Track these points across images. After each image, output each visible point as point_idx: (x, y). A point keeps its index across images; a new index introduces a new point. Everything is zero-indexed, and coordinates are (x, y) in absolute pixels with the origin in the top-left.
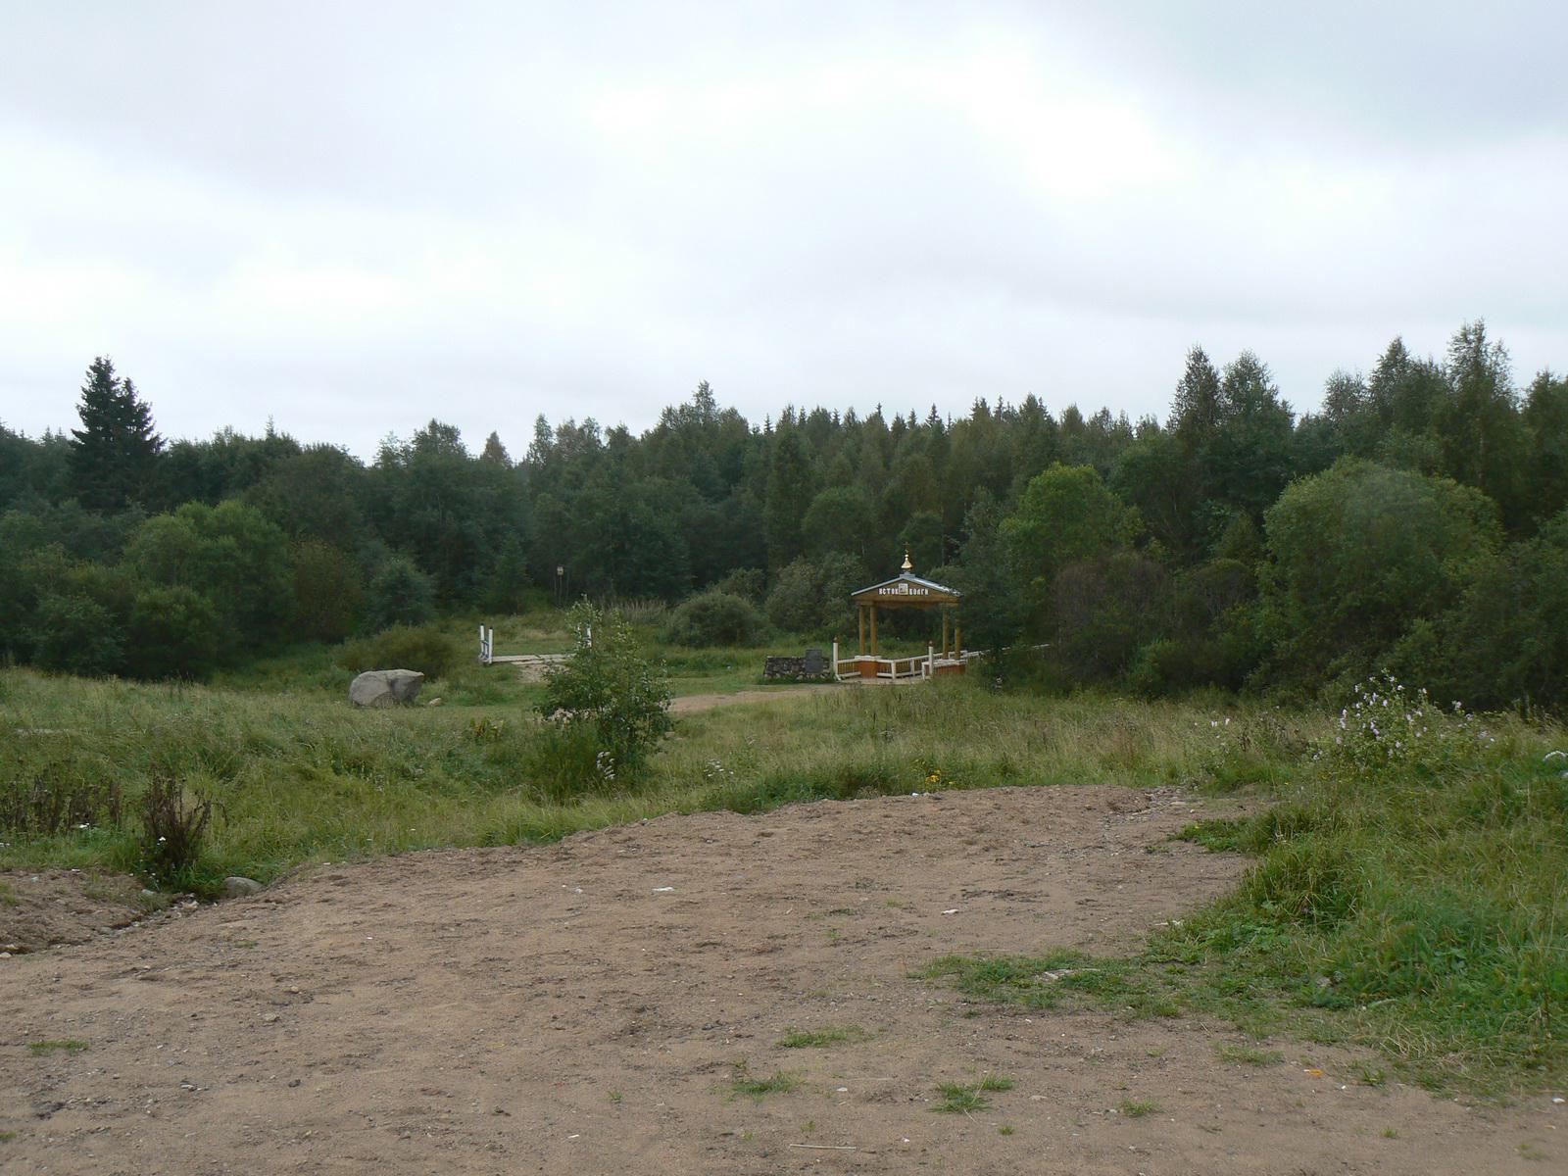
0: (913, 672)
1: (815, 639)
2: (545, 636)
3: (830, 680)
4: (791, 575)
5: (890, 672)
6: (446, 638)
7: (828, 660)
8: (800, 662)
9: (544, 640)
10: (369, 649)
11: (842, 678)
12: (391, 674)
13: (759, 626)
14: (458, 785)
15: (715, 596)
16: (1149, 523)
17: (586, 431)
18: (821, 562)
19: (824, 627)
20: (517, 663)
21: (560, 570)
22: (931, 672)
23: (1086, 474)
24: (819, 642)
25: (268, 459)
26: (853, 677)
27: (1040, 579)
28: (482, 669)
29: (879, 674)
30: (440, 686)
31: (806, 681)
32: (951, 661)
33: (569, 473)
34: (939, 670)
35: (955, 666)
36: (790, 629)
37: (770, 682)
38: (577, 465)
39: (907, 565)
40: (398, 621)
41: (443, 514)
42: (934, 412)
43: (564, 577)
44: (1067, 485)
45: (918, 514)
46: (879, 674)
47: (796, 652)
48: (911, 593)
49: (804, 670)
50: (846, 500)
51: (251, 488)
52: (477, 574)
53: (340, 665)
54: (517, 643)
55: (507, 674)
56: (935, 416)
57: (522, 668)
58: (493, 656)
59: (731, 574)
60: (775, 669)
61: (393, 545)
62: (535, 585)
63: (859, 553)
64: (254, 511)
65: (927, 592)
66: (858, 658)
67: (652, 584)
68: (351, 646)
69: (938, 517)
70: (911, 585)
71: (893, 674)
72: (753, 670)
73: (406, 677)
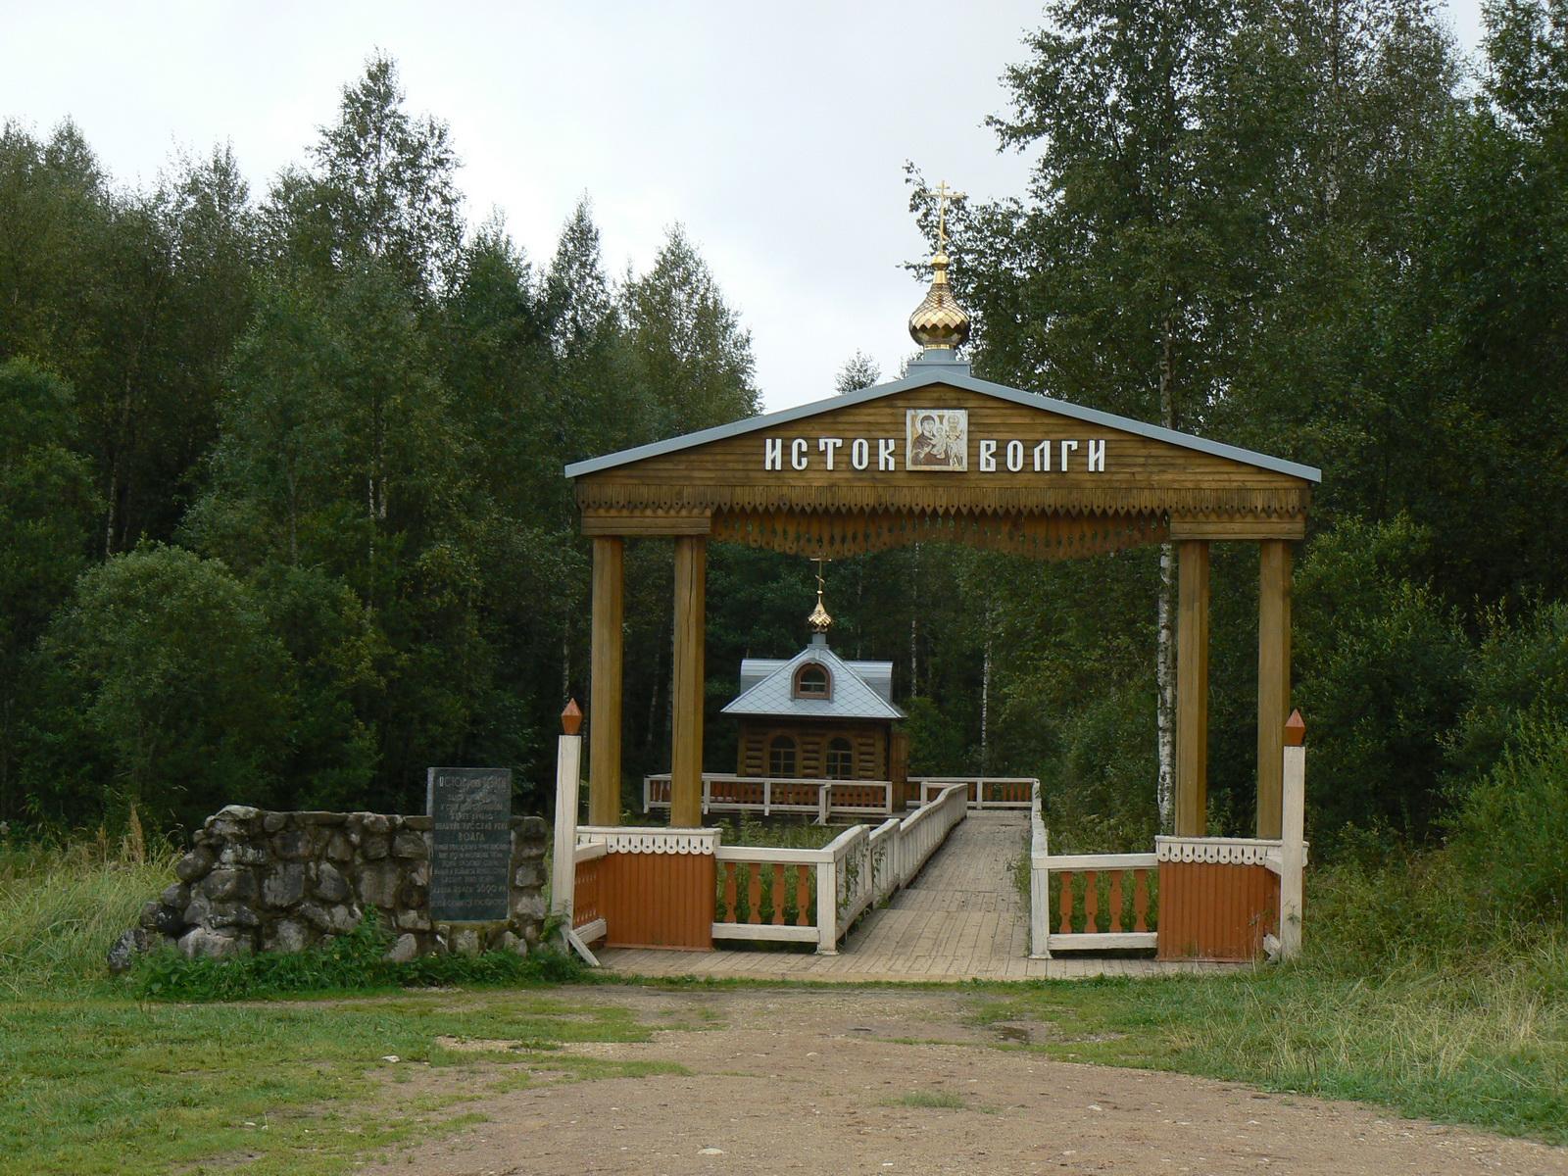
16: (37, 763)
48: (987, 463)
60: (276, 891)
65: (1097, 457)
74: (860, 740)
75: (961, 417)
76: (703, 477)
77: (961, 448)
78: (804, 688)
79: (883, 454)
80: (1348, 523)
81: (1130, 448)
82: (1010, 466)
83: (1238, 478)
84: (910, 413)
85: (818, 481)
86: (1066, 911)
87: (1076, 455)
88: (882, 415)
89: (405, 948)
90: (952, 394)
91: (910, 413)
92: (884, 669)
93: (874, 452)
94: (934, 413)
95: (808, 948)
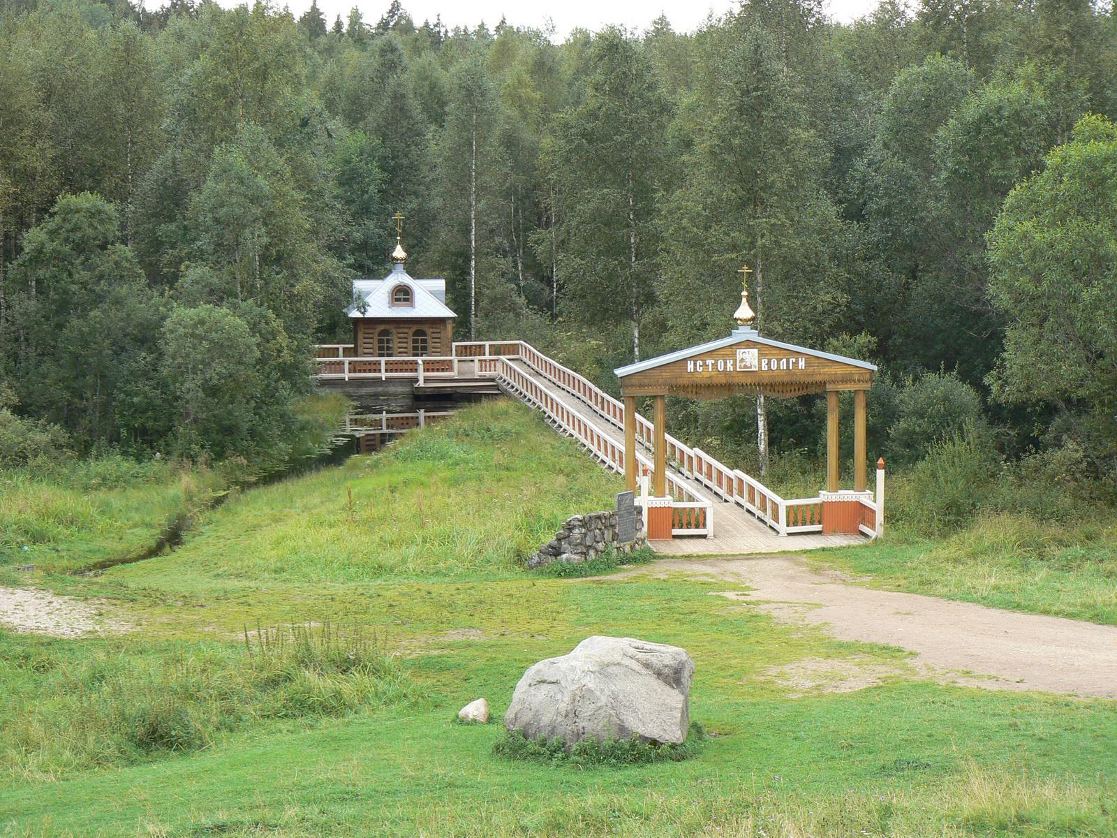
29: (676, 532)
46: (676, 532)
65: (802, 364)
74: (431, 330)
75: (756, 351)
77: (756, 362)
78: (397, 300)
79: (729, 365)
80: (845, 336)
81: (813, 360)
82: (772, 368)
83: (849, 370)
84: (738, 351)
85: (706, 375)
86: (792, 520)
88: (728, 352)
90: (751, 343)
91: (738, 351)
92: (440, 284)
93: (725, 364)
94: (746, 350)
95: (704, 537)
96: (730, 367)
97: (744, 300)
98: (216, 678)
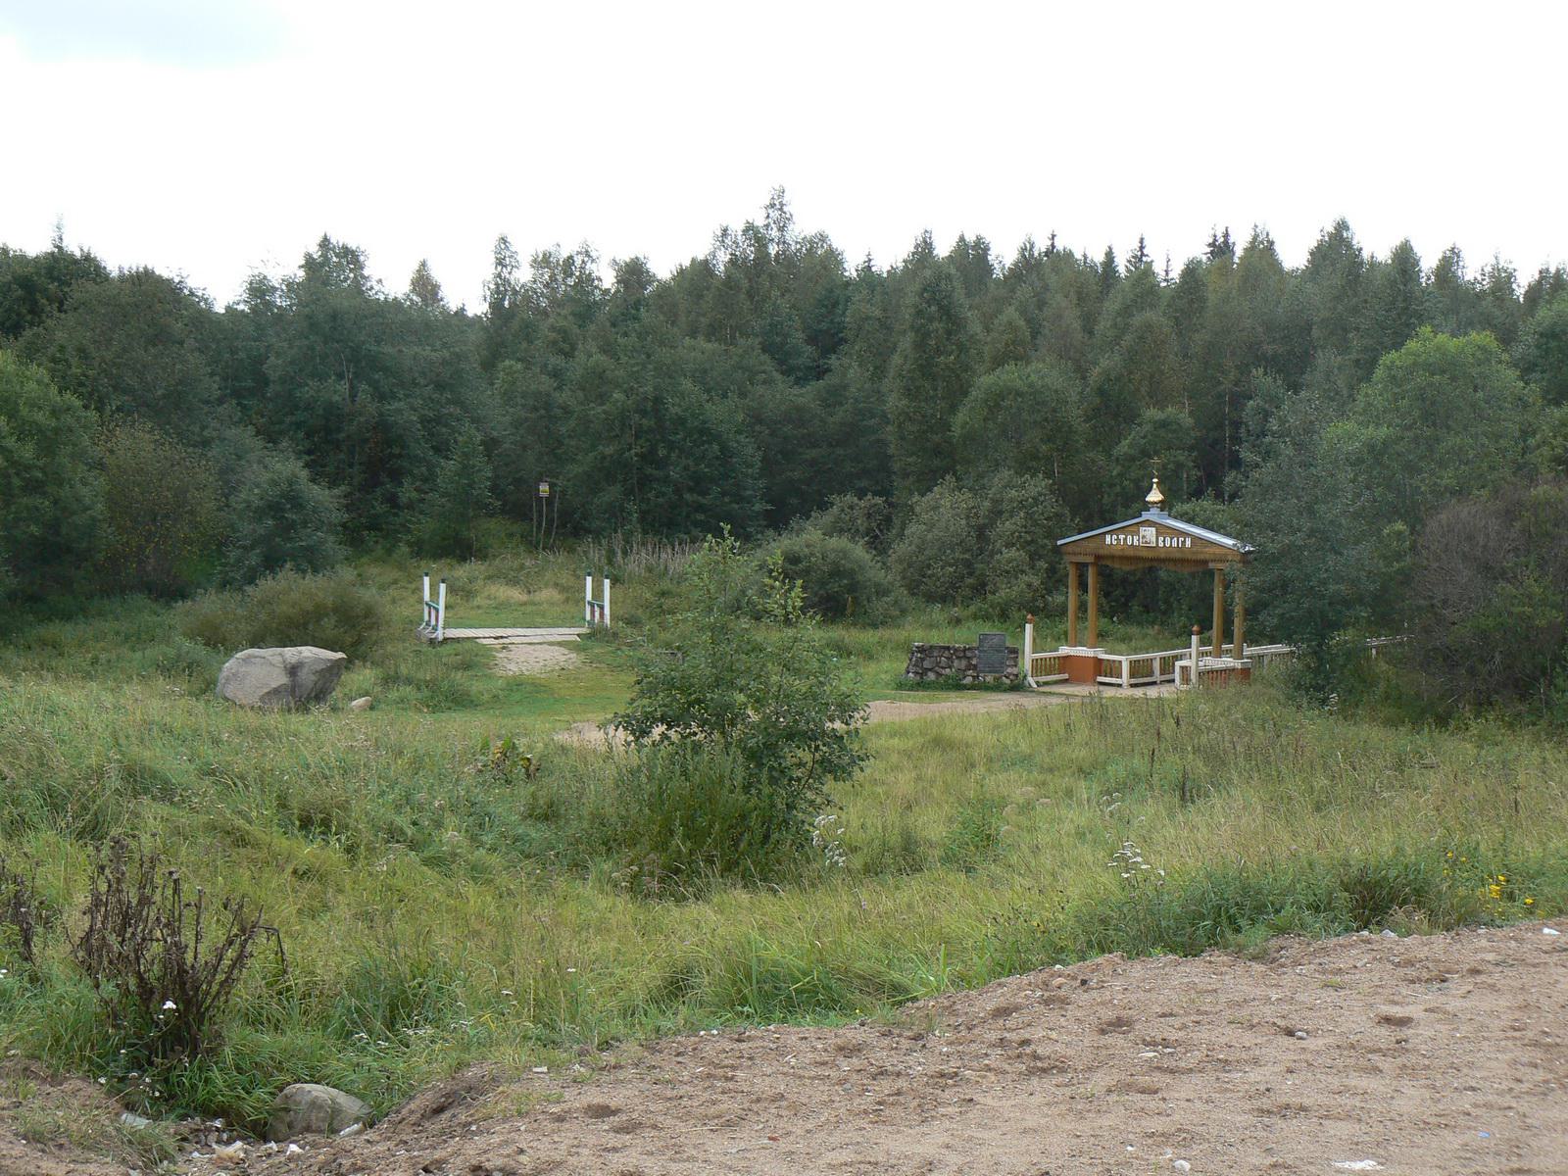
0: (1157, 676)
1: (975, 617)
2: (524, 598)
3: (1017, 686)
4: (935, 508)
5: (1119, 676)
6: (368, 595)
7: (1015, 653)
8: (969, 654)
9: (525, 604)
10: (239, 611)
11: (1037, 683)
12: (291, 653)
13: (882, 591)
14: (494, 860)
15: (811, 537)
17: (578, 261)
18: (983, 487)
19: (990, 597)
20: (485, 642)
21: (544, 489)
22: (1193, 677)
23: (1482, 348)
24: (980, 621)
25: (53, 287)
26: (1056, 682)
27: (1400, 526)
28: (425, 648)
29: (1100, 679)
30: (364, 676)
31: (979, 687)
32: (1227, 662)
33: (553, 328)
34: (1207, 675)
35: (1234, 669)
36: (931, 598)
37: (921, 685)
38: (566, 317)
39: (1155, 496)
40: (288, 566)
41: (352, 387)
42: (1142, 248)
43: (550, 500)
44: (1448, 367)
45: (1152, 413)
46: (1100, 679)
47: (963, 636)
49: (975, 667)
50: (1031, 385)
51: (28, 333)
52: (407, 492)
53: (191, 635)
54: (479, 607)
55: (472, 658)
56: (1142, 255)
57: (497, 651)
58: (444, 628)
59: (832, 504)
60: (927, 664)
61: (270, 437)
62: (503, 512)
63: (1049, 475)
64: (38, 371)
65: (1188, 543)
66: (1065, 650)
67: (701, 517)
68: (209, 604)
69: (1186, 419)
70: (1162, 530)
71: (1125, 679)
72: (886, 665)
73: (318, 660)
75: (1154, 529)
76: (1092, 545)
87: (1184, 542)
89: (968, 680)
96: (1136, 543)
97: (1155, 486)
98: (161, 295)
